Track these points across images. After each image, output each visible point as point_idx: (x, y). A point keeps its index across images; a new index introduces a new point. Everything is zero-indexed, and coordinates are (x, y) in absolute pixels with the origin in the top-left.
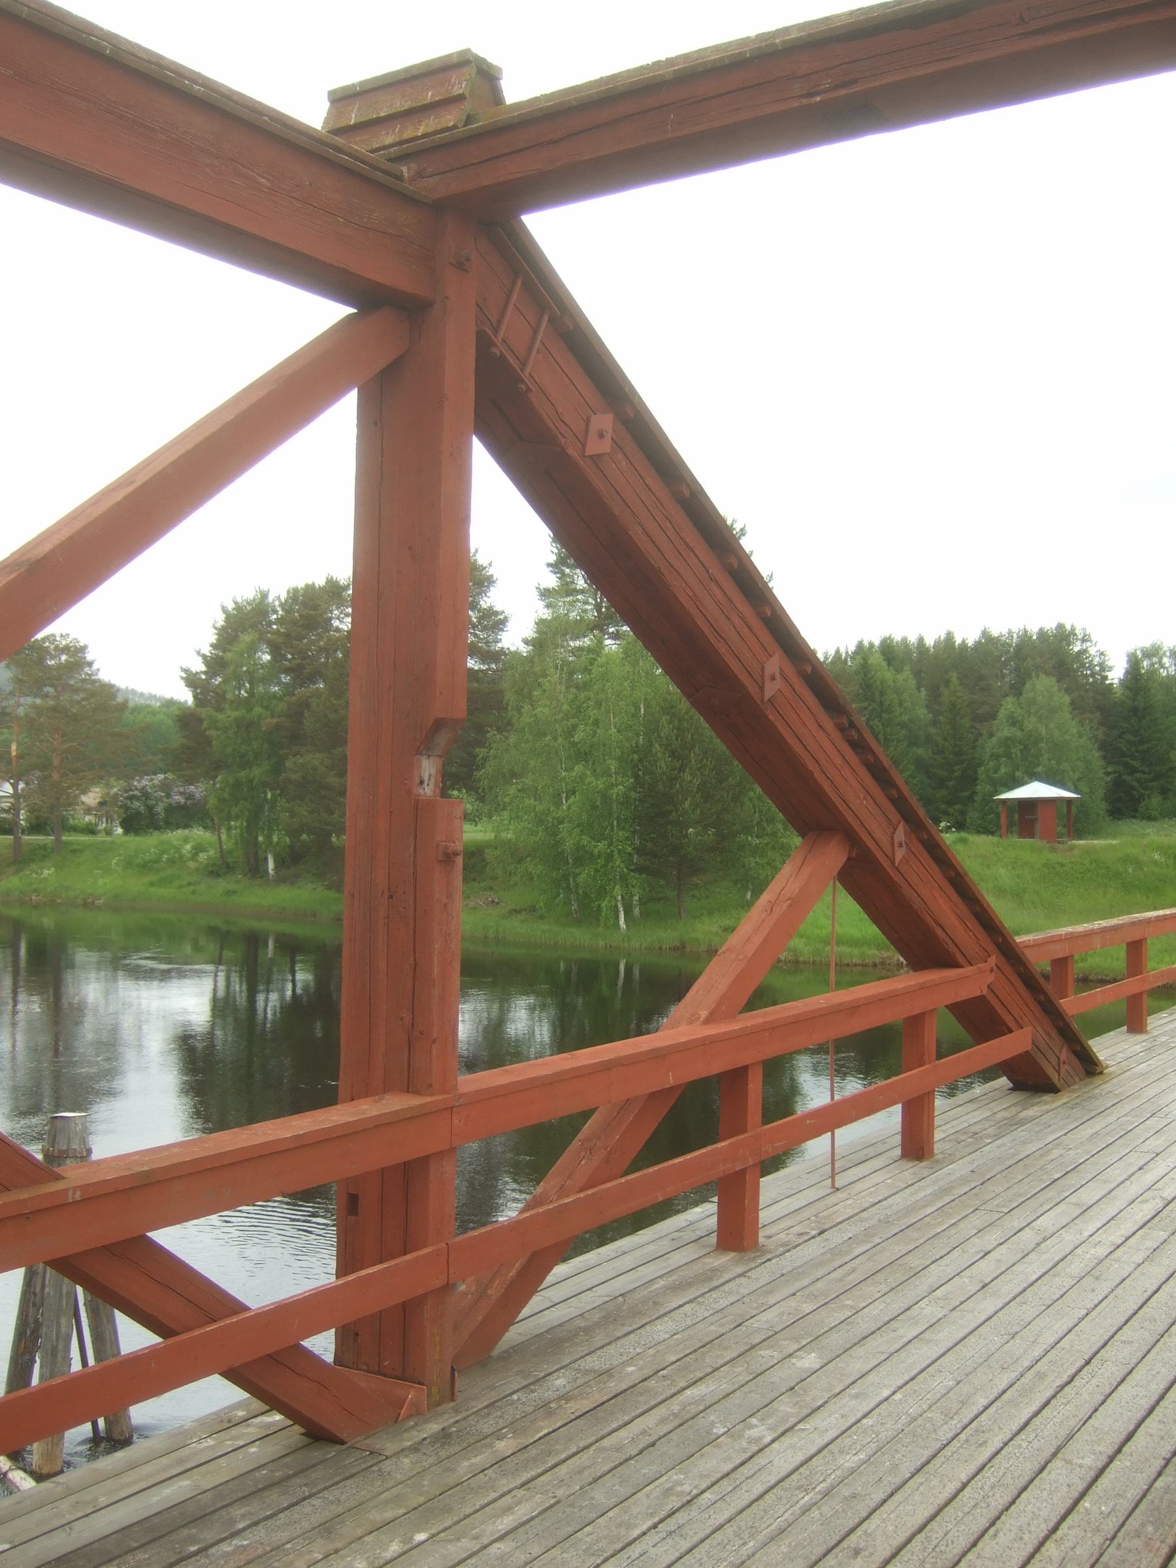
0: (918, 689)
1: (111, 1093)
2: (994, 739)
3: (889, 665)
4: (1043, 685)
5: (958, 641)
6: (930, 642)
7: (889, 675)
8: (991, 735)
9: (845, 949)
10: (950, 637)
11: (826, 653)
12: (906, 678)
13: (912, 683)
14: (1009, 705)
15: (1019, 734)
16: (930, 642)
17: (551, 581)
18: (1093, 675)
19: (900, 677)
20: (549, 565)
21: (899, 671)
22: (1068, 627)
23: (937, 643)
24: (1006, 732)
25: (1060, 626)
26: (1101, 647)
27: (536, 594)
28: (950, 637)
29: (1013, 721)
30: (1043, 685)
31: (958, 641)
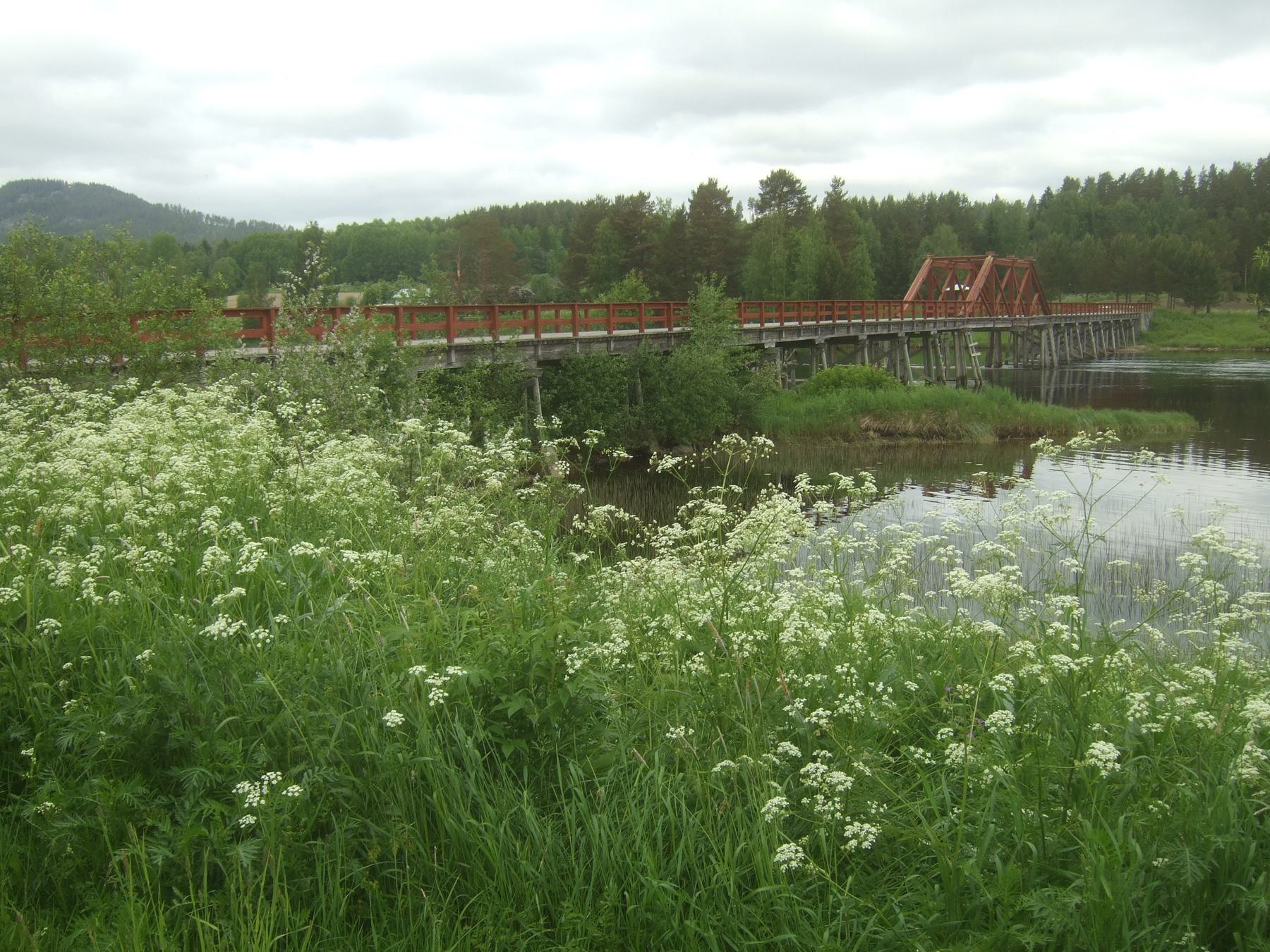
4: (944, 230)
6: (879, 200)
10: (890, 198)
12: (869, 225)
13: (873, 227)
16: (879, 200)
21: (866, 220)
23: (884, 202)
25: (951, 193)
28: (890, 198)
30: (944, 230)
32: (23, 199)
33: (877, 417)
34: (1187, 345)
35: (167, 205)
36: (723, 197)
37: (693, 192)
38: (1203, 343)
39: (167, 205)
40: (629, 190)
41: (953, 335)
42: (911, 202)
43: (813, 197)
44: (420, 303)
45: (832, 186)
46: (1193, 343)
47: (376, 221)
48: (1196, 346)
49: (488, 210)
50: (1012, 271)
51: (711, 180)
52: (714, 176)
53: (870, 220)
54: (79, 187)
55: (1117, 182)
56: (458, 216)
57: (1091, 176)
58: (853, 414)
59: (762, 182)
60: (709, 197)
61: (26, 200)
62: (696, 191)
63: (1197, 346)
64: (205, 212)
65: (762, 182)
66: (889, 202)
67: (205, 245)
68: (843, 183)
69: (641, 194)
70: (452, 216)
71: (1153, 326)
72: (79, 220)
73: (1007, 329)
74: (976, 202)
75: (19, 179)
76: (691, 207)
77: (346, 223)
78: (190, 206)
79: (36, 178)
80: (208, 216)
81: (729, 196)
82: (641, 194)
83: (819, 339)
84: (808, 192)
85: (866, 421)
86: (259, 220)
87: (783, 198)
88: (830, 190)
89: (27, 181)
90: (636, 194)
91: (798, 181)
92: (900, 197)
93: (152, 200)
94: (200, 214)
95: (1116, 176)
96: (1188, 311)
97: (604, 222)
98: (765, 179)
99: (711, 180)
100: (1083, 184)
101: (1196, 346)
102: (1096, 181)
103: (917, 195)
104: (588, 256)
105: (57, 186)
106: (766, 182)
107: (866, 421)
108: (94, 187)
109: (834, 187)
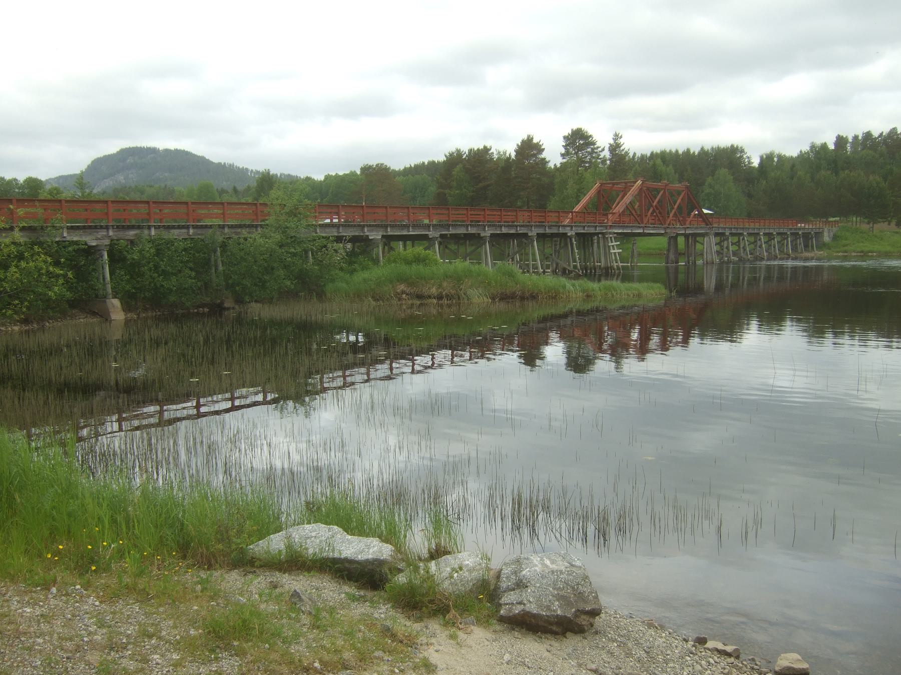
0: (675, 174)
1: (718, 147)
2: (703, 194)
3: (664, 164)
4: (723, 172)
5: (692, 152)
6: (680, 152)
7: (664, 168)
8: (703, 192)
9: (651, 251)
10: (688, 150)
11: (635, 154)
12: (670, 169)
14: (709, 180)
15: (713, 191)
16: (680, 152)
17: (563, 151)
18: (745, 166)
19: (668, 169)
20: (563, 146)
21: (667, 166)
22: (735, 146)
23: (683, 153)
24: (707, 191)
26: (748, 155)
27: (560, 155)
28: (688, 150)
29: (711, 186)
30: (723, 172)
31: (692, 152)
32: (130, 160)
33: (411, 284)
34: (854, 252)
35: (225, 163)
36: (539, 149)
37: (518, 145)
38: (866, 249)
39: (225, 163)
40: (478, 145)
41: (598, 237)
42: (703, 152)
43: (602, 147)
44: (68, 199)
45: (613, 139)
46: (859, 250)
47: (351, 172)
48: (861, 252)
49: (426, 163)
50: (664, 192)
51: (529, 136)
52: (531, 133)
53: (671, 167)
54: (167, 151)
55: (876, 138)
56: (405, 168)
57: (857, 134)
58: (391, 282)
59: (564, 137)
60: (529, 148)
61: (132, 161)
62: (520, 144)
63: (862, 252)
64: (250, 168)
65: (564, 137)
66: (687, 153)
67: (235, 190)
68: (621, 137)
69: (485, 147)
70: (402, 168)
71: (835, 238)
72: (166, 174)
73: (682, 234)
74: (766, 155)
75: (128, 147)
76: (516, 156)
77: (330, 174)
78: (240, 164)
79: (139, 146)
80: (252, 170)
81: (543, 147)
82: (485, 147)
83: (432, 234)
84: (598, 144)
85: (402, 287)
86: (286, 173)
87: (580, 148)
88: (612, 142)
89: (133, 148)
90: (481, 147)
91: (591, 136)
92: (695, 150)
93: (215, 160)
94: (247, 169)
95: (876, 134)
96: (865, 227)
97: (460, 166)
98: (567, 135)
99: (529, 136)
100: (850, 140)
101: (861, 252)
102: (860, 138)
103: (708, 147)
104: (447, 191)
105: (153, 151)
106: (568, 137)
107: (402, 287)
108: (177, 151)
109: (615, 140)
